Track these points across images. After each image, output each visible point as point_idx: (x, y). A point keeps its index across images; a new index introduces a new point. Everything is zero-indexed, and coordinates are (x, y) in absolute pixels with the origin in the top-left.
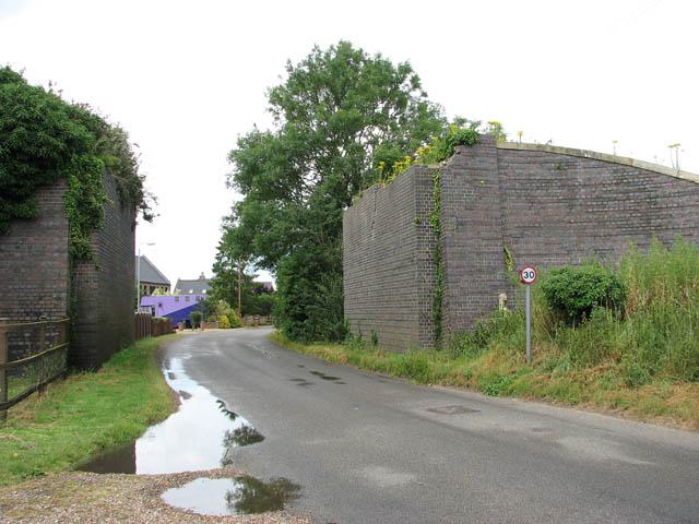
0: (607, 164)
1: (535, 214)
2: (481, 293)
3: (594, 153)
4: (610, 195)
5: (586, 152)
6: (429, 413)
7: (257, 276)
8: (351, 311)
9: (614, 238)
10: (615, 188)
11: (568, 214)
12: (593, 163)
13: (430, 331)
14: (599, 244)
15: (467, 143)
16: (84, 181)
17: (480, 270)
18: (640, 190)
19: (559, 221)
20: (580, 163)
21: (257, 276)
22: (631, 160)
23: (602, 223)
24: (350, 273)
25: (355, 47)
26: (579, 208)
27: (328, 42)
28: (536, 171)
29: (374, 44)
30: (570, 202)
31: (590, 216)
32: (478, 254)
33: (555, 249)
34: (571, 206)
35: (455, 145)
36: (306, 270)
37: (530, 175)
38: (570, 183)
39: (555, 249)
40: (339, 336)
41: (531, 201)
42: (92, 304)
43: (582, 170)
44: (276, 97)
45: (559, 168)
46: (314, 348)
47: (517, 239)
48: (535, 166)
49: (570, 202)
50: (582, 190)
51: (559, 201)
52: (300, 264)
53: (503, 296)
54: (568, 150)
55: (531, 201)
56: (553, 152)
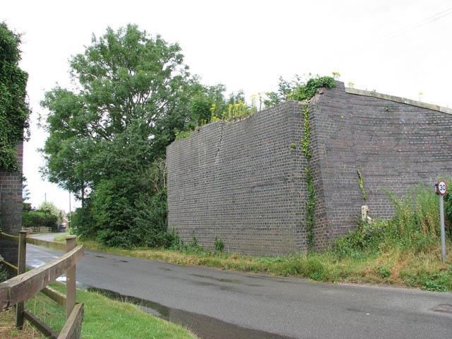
0: (421, 109)
1: (375, 144)
2: (346, 205)
3: (411, 101)
4: (425, 132)
5: (406, 99)
6: (435, 313)
7: (28, 198)
8: (173, 223)
9: (430, 164)
10: (428, 127)
11: (397, 145)
12: (411, 108)
13: (303, 238)
14: (420, 168)
15: (329, 87)
16: (13, 92)
17: (344, 187)
18: (446, 129)
19: (391, 150)
20: (402, 107)
21: (28, 198)
22: (438, 107)
23: (420, 152)
24: (172, 191)
25: (140, 29)
26: (404, 141)
27: (119, 25)
28: (374, 113)
29: (151, 29)
30: (397, 136)
31: (412, 147)
32: (342, 174)
33: (390, 171)
34: (398, 139)
35: (319, 87)
36: (125, 191)
37: (368, 114)
38: (396, 122)
39: (390, 171)
40: (169, 243)
41: (371, 134)
42: (16, 217)
43: (404, 113)
44: (78, 64)
45: (387, 111)
46: (139, 252)
47: (364, 162)
48: (371, 108)
49: (397, 136)
50: (405, 128)
51: (390, 135)
52: (117, 188)
53: (365, 208)
54: (392, 97)
55: (371, 134)
56: (382, 98)
